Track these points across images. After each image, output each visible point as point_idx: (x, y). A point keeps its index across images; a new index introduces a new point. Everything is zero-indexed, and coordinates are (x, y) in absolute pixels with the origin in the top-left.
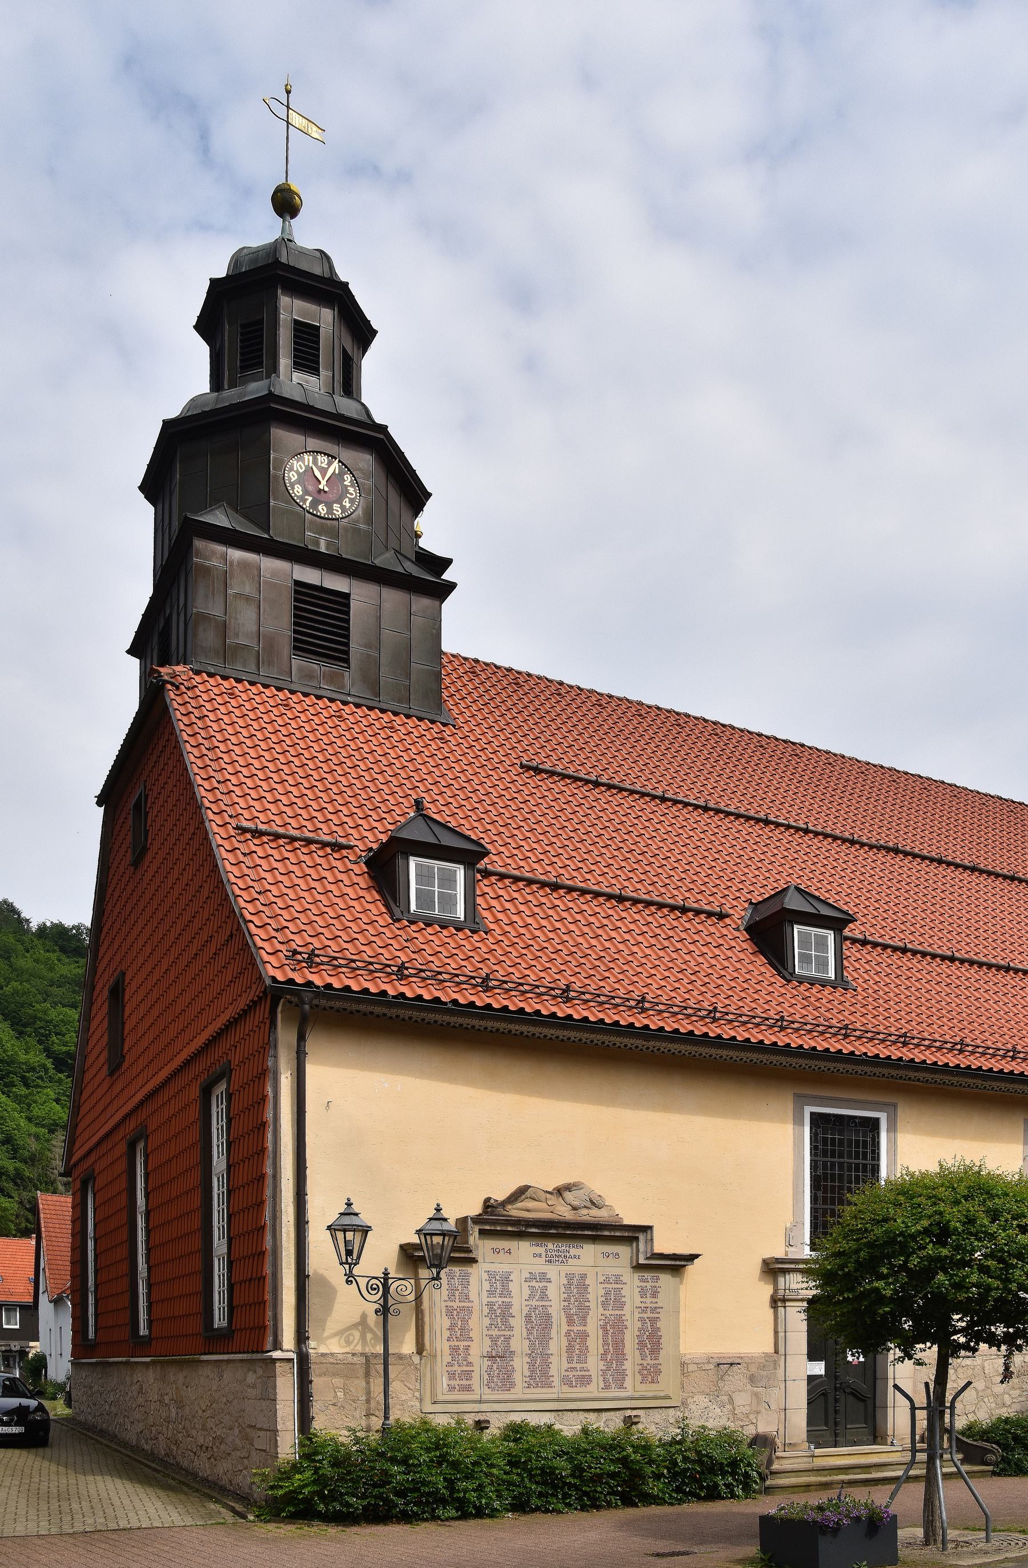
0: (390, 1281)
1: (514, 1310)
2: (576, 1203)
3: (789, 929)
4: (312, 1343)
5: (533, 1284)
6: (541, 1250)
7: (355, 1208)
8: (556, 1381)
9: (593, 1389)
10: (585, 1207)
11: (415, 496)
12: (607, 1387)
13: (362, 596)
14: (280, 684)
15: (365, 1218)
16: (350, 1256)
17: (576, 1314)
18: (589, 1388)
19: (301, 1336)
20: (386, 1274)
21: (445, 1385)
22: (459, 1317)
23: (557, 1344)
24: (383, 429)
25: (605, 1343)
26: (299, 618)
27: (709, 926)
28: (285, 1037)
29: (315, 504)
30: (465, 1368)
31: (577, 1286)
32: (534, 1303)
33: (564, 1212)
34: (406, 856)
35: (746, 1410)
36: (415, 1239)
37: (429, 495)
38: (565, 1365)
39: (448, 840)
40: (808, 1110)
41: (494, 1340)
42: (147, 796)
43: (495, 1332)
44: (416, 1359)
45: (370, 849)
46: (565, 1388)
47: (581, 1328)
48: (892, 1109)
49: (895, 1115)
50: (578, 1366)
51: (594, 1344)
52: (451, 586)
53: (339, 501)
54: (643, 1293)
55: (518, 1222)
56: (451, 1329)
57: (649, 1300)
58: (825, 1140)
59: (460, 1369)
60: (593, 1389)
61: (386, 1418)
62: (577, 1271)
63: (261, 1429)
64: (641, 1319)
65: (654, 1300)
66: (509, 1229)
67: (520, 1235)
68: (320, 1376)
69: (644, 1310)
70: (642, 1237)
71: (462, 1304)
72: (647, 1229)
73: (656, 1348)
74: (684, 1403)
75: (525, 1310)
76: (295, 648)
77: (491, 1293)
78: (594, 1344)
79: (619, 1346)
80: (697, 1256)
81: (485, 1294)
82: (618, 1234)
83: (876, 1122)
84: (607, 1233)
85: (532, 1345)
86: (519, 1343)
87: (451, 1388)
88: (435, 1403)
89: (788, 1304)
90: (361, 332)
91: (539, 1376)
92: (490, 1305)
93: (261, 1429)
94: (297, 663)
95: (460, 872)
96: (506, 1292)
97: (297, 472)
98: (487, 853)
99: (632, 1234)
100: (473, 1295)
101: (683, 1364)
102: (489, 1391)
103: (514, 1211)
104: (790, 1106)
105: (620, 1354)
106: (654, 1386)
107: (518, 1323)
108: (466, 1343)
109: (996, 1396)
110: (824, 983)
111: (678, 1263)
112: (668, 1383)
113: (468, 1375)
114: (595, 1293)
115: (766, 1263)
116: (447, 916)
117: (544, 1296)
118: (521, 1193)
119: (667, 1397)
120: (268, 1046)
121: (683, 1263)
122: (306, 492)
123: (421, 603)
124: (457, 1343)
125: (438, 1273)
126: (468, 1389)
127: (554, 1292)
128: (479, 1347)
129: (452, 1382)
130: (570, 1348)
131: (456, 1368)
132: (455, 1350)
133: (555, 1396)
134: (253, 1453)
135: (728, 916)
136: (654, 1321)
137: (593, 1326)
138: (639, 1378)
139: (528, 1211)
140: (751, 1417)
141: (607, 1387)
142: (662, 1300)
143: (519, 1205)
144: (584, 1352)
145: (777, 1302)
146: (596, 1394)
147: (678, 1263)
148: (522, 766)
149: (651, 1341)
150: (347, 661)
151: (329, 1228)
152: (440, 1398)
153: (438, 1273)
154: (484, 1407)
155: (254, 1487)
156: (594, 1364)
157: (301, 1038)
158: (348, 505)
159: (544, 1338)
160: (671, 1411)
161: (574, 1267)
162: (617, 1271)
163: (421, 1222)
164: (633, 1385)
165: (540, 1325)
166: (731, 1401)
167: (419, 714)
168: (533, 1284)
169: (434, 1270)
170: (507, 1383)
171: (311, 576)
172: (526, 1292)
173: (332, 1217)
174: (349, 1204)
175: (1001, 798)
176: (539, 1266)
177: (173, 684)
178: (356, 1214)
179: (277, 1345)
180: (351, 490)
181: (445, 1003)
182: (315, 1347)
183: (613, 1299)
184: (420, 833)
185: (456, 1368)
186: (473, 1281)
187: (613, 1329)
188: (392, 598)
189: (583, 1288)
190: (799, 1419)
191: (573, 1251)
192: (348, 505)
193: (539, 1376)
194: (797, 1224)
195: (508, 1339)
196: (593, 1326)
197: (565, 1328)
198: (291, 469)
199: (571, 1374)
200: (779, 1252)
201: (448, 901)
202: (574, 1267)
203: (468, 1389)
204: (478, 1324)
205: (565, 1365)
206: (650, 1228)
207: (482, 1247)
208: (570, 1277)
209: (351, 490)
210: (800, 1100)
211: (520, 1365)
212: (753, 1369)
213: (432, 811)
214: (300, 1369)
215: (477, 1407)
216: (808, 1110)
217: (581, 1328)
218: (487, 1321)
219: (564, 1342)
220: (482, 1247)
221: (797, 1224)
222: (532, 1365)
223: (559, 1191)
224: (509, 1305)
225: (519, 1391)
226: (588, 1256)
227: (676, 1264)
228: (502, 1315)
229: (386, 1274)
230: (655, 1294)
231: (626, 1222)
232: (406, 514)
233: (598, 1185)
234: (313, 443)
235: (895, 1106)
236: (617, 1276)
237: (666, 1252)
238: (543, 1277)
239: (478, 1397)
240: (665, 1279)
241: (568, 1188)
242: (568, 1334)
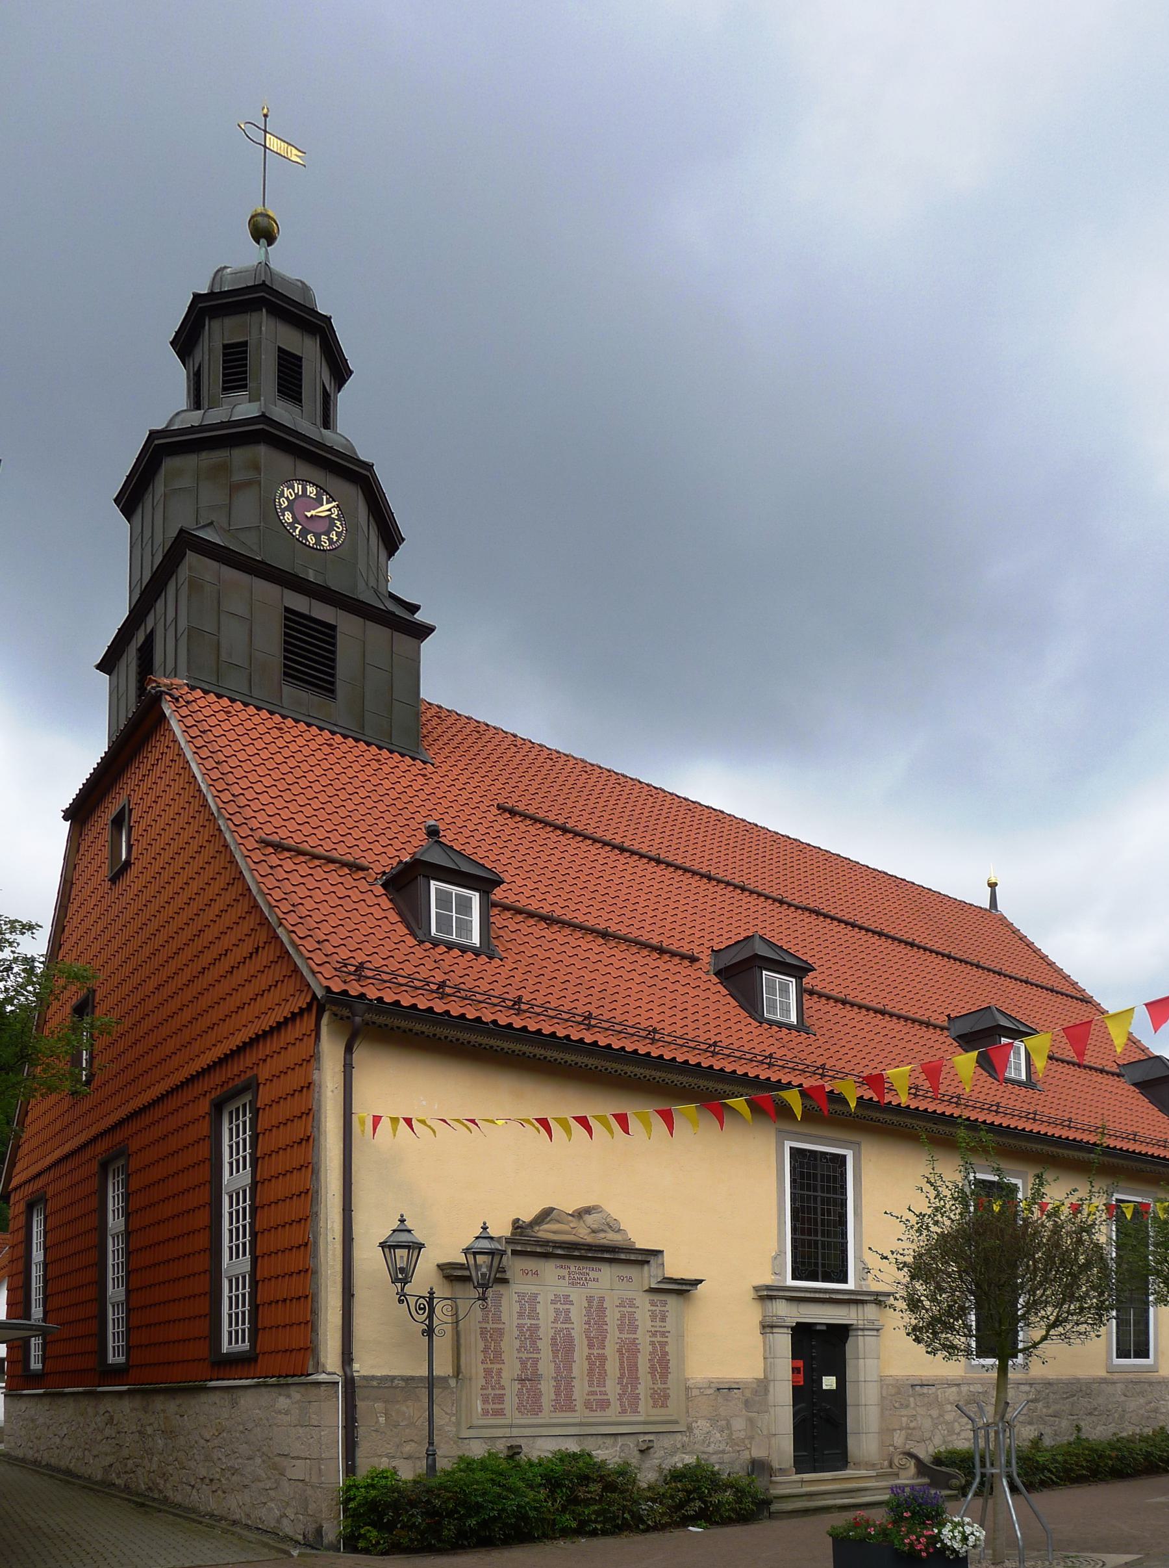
0: (435, 1301)
1: (541, 1333)
2: (595, 1226)
3: (758, 975)
4: (356, 1366)
5: (558, 1306)
6: (565, 1272)
7: (409, 1224)
8: (579, 1405)
9: (612, 1413)
10: (603, 1230)
11: (391, 539)
12: (624, 1411)
13: (347, 625)
14: (272, 708)
15: (418, 1236)
16: (402, 1276)
17: (597, 1338)
18: (609, 1412)
19: (347, 1357)
20: (431, 1293)
21: (479, 1409)
22: (492, 1337)
23: (579, 1367)
24: (369, 467)
25: (622, 1367)
26: (290, 647)
27: (684, 968)
28: (331, 1052)
29: (304, 532)
30: (498, 1392)
31: (596, 1310)
32: (559, 1325)
33: (582, 1234)
34: (428, 878)
35: (742, 1435)
36: (462, 1259)
37: (403, 540)
38: (587, 1388)
39: (466, 868)
40: (788, 1145)
41: (523, 1363)
42: (130, 811)
43: (524, 1355)
44: (453, 1383)
45: (384, 873)
46: (587, 1413)
47: (600, 1351)
48: (856, 1146)
49: (860, 1152)
50: (598, 1389)
51: (612, 1367)
52: (429, 630)
53: (327, 533)
54: (653, 1318)
55: (547, 1243)
56: (485, 1351)
57: (658, 1324)
58: (802, 1173)
59: (493, 1392)
60: (612, 1413)
61: (350, 1470)
62: (597, 1294)
63: (298, 1458)
64: (652, 1343)
65: (663, 1324)
66: (538, 1250)
67: (546, 1256)
68: (363, 1400)
69: (654, 1334)
70: (652, 1260)
71: (495, 1326)
72: (657, 1253)
73: (664, 1375)
74: (690, 1429)
75: (551, 1333)
76: (285, 674)
77: (521, 1315)
78: (612, 1367)
79: (634, 1368)
80: (701, 1281)
81: (515, 1316)
82: (633, 1257)
83: (843, 1158)
84: (623, 1256)
85: (557, 1368)
86: (546, 1367)
87: (485, 1412)
88: (470, 1427)
89: (775, 1330)
90: (340, 372)
91: (565, 1403)
92: (519, 1326)
93: (298, 1458)
94: (286, 689)
95: (476, 898)
96: (533, 1314)
97: (287, 498)
98: (499, 882)
99: (647, 1257)
100: (505, 1318)
101: (688, 1389)
102: (519, 1415)
103: (545, 1232)
104: (773, 1140)
105: (635, 1380)
106: (663, 1411)
107: (544, 1345)
108: (499, 1366)
109: (947, 1423)
110: (789, 1027)
111: (684, 1287)
112: (674, 1408)
113: (500, 1398)
114: (612, 1317)
115: (756, 1289)
116: (463, 941)
117: (568, 1320)
118: (546, 1215)
119: (676, 1422)
120: (312, 1059)
121: (688, 1288)
122: (295, 520)
123: (403, 641)
124: (490, 1366)
125: (484, 1293)
126: (499, 1413)
127: (577, 1315)
128: (510, 1369)
129: (487, 1406)
130: (591, 1372)
131: (490, 1391)
132: (488, 1372)
133: (577, 1420)
134: (285, 1483)
135: (697, 960)
136: (663, 1344)
137: (610, 1350)
138: (651, 1402)
139: (554, 1232)
140: (747, 1442)
141: (624, 1411)
142: (670, 1325)
143: (545, 1227)
144: (603, 1374)
145: (767, 1327)
146: (614, 1419)
147: (684, 1287)
148: (499, 807)
149: (661, 1365)
150: (332, 691)
151: (383, 1245)
152: (476, 1422)
153: (484, 1293)
154: (515, 1432)
155: (285, 1521)
156: (612, 1388)
157: (349, 1050)
158: (335, 538)
159: (568, 1361)
160: (679, 1437)
161: (594, 1289)
162: (630, 1294)
163: (467, 1241)
164: (645, 1412)
165: (564, 1347)
166: (729, 1426)
167: (400, 750)
168: (558, 1306)
169: (480, 1290)
170: (536, 1409)
171: (299, 603)
172: (552, 1315)
173: (384, 1233)
174: (402, 1221)
175: (886, 874)
176: (564, 1288)
177: (170, 695)
178: (409, 1231)
179: (318, 1367)
180: (338, 524)
181: (487, 1023)
182: (362, 1367)
183: (628, 1324)
184: (437, 857)
185: (490, 1391)
186: (504, 1302)
187: (629, 1351)
188: (377, 633)
189: (602, 1310)
190: (786, 1444)
191: (593, 1275)
192: (335, 538)
193: (565, 1403)
194: (781, 1253)
195: (536, 1361)
196: (610, 1350)
197: (586, 1351)
198: (282, 495)
199: (592, 1398)
200: (768, 1279)
201: (464, 927)
202: (594, 1289)
203: (499, 1413)
204: (510, 1345)
205: (587, 1388)
206: (661, 1252)
207: (516, 1267)
208: (590, 1299)
209: (338, 524)
210: (781, 1136)
211: (547, 1388)
212: (748, 1394)
213: (447, 838)
214: (345, 1393)
215: (507, 1432)
216: (788, 1145)
217: (600, 1351)
218: (517, 1343)
219: (586, 1365)
220: (516, 1267)
221: (781, 1253)
222: (557, 1387)
223: (580, 1214)
224: (537, 1327)
225: (545, 1416)
226: (605, 1277)
227: (683, 1288)
228: (530, 1336)
229: (431, 1293)
230: (663, 1319)
231: (638, 1246)
232: (383, 554)
233: (614, 1209)
234: (304, 470)
235: (859, 1144)
236: (632, 1300)
237: (675, 1277)
238: (567, 1300)
239: (508, 1422)
240: (672, 1302)
241: (588, 1211)
242: (588, 1358)
